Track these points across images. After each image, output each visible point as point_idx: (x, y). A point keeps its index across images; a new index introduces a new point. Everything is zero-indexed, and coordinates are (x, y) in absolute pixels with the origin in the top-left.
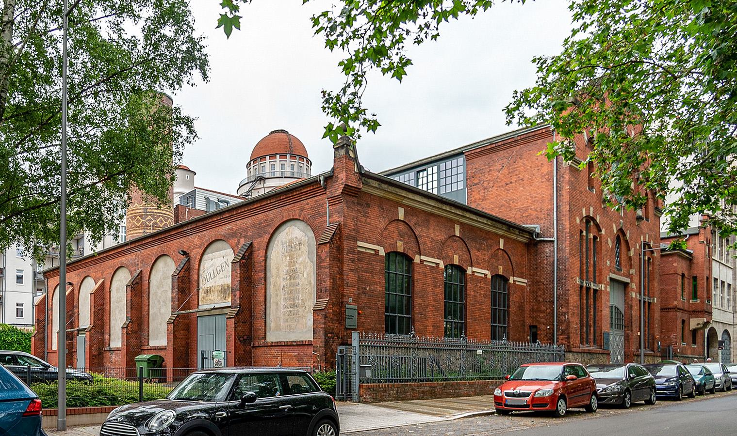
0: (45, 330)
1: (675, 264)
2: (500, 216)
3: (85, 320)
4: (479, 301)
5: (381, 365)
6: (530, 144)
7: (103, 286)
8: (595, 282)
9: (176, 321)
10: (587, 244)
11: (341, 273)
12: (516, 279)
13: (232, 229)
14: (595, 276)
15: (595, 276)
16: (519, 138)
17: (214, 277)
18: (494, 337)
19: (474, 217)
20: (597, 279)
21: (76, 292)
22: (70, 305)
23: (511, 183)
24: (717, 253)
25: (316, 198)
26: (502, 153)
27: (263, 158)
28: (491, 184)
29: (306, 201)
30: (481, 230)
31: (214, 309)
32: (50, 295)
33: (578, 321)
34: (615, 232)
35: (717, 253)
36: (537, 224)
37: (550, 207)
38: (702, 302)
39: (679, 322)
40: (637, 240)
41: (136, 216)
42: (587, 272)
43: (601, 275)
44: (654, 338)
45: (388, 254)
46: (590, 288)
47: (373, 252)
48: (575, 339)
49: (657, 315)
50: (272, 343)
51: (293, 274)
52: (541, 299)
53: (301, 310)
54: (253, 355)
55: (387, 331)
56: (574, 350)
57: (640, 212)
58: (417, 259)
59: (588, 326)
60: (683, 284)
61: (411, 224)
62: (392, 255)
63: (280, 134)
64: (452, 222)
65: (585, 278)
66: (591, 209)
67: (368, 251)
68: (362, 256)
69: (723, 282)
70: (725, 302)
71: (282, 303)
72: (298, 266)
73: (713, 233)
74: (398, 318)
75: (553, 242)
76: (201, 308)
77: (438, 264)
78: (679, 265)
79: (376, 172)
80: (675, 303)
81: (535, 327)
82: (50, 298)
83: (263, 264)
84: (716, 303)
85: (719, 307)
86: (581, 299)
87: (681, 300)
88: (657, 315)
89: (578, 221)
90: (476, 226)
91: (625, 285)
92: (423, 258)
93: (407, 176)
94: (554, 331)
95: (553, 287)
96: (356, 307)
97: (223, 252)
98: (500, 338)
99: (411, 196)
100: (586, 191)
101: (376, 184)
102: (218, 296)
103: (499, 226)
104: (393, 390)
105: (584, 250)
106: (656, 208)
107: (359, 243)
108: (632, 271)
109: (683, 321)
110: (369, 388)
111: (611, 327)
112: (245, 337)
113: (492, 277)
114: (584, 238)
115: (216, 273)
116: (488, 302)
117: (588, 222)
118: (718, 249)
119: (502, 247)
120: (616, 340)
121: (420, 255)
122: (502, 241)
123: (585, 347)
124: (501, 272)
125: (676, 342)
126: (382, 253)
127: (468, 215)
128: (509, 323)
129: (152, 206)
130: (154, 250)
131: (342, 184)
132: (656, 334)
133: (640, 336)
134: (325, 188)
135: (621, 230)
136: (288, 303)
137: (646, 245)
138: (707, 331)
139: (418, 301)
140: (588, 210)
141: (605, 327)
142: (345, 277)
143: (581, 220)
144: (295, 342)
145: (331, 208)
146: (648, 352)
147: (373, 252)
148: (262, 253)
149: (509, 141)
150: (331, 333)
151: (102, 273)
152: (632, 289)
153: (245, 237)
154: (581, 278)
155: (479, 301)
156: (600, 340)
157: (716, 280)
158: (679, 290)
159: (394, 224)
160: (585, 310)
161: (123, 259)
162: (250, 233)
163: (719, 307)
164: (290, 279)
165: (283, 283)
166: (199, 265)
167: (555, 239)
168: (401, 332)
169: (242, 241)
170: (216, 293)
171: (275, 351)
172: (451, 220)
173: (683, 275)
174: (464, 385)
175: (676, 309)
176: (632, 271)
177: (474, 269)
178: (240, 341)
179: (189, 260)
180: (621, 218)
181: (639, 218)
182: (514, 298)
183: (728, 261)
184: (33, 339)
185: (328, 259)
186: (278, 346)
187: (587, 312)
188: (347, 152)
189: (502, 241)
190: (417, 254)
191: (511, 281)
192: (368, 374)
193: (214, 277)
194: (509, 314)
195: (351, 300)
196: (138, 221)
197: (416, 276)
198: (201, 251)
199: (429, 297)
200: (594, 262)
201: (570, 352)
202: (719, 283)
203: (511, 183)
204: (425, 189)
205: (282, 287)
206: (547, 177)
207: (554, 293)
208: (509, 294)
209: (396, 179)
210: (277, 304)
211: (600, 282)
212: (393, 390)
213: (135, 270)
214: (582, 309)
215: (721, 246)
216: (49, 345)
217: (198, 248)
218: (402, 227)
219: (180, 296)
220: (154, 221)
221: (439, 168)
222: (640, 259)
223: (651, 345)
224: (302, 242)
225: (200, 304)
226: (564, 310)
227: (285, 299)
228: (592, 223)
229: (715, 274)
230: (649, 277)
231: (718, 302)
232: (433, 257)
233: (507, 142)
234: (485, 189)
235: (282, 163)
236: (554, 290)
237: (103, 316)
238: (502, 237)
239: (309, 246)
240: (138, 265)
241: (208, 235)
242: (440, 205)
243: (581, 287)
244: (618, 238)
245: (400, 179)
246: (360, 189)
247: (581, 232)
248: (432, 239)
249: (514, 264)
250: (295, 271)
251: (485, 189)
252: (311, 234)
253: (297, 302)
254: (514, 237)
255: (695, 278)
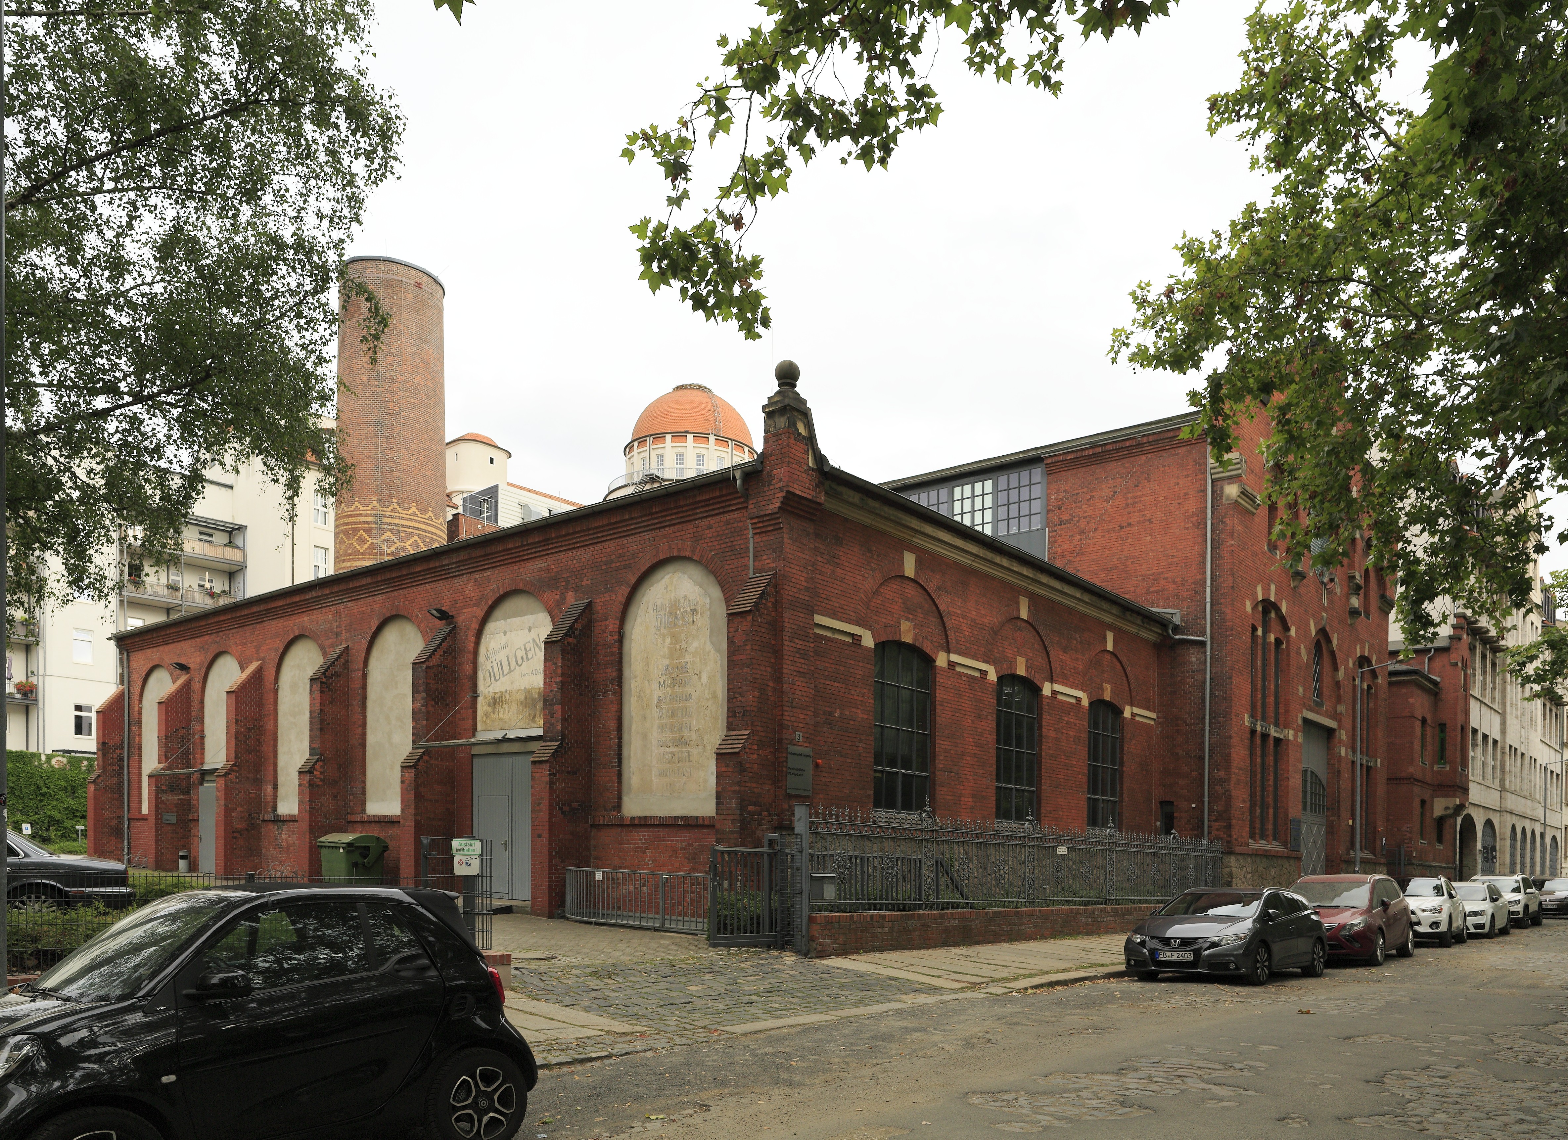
0: (122, 768)
1: (1411, 700)
2: (1109, 587)
3: (216, 751)
4: (966, 740)
5: (863, 872)
6: (1165, 454)
7: (256, 678)
8: (1277, 725)
9: (421, 764)
10: (1264, 654)
11: (778, 677)
12: (1136, 710)
13: (548, 569)
14: (1277, 714)
15: (1277, 714)
16: (1145, 440)
17: (510, 671)
18: (1094, 820)
19: (1057, 584)
20: (1282, 720)
21: (196, 686)
22: (183, 715)
23: (1130, 525)
24: (1478, 684)
25: (727, 517)
26: (1114, 467)
27: (659, 437)
28: (1093, 525)
29: (705, 522)
30: (1070, 610)
31: (504, 740)
32: (136, 689)
33: (1246, 796)
34: (1314, 633)
35: (1478, 684)
36: (1176, 607)
37: (1199, 577)
38: (1454, 770)
39: (1417, 803)
40: (1347, 649)
41: (356, 531)
42: (1264, 705)
43: (1287, 711)
44: (1375, 831)
45: (881, 646)
46: (1268, 735)
47: (849, 640)
48: (1240, 830)
49: (1381, 789)
50: (633, 818)
51: (677, 676)
52: (1181, 752)
53: (695, 752)
54: (593, 843)
55: (877, 804)
56: (1238, 849)
57: (1355, 602)
58: (941, 660)
59: (1264, 806)
60: (1423, 736)
61: (931, 588)
62: (888, 648)
63: (695, 393)
64: (1012, 592)
65: (1259, 715)
66: (1273, 587)
67: (837, 636)
68: (824, 646)
69: (1485, 737)
70: (1489, 770)
71: (655, 736)
72: (688, 658)
73: (1472, 649)
74: (903, 779)
75: (1203, 644)
76: (481, 736)
77: (984, 673)
78: (1419, 703)
79: (875, 482)
80: (1411, 769)
81: (1171, 803)
82: (136, 697)
83: (615, 650)
84: (1475, 773)
85: (1478, 778)
86: (1252, 754)
87: (1421, 764)
88: (1381, 789)
89: (1249, 608)
90: (1052, 596)
91: (1330, 732)
92: (954, 658)
93: (933, 494)
94: (1203, 812)
95: (1203, 730)
96: (808, 751)
97: (529, 619)
98: (1104, 825)
99: (929, 529)
100: (1264, 553)
101: (855, 497)
102: (519, 713)
103: (1105, 605)
104: (882, 927)
105: (1259, 663)
106: (1383, 597)
107: (819, 619)
108: (1341, 708)
109: (1423, 802)
110: (829, 922)
111: (1305, 809)
112: (575, 805)
113: (1091, 704)
114: (1260, 641)
115: (513, 664)
116: (1083, 752)
117: (1265, 612)
118: (1479, 677)
119: (1110, 647)
120: (1312, 833)
121: (948, 651)
122: (1110, 637)
123: (1262, 845)
124: (1107, 697)
125: (1411, 839)
126: (868, 641)
127: (1044, 579)
128: (1121, 795)
129: (394, 510)
130: (377, 604)
131: (781, 489)
132: (1379, 823)
133: (1353, 828)
134: (746, 495)
135: (1323, 632)
136: (668, 735)
137: (1364, 661)
138: (1459, 820)
139: (942, 744)
140: (1266, 589)
141: (1294, 810)
142: (786, 687)
143: (1254, 608)
144: (682, 818)
145: (758, 538)
146: (1368, 855)
147: (849, 640)
148: (612, 625)
149: (1128, 444)
150: (755, 804)
151: (258, 649)
152: (1340, 741)
153: (576, 589)
154: (1252, 716)
155: (1064, 752)
156: (1286, 832)
157: (1475, 731)
158: (1417, 746)
159: (894, 585)
160: (1259, 776)
161: (305, 620)
162: (586, 582)
163: (1478, 778)
164: (673, 685)
165: (657, 693)
166: (477, 643)
167: (1207, 638)
168: (907, 806)
169: (570, 597)
170: (514, 707)
171: (639, 837)
172: (1011, 587)
173: (1424, 721)
174: (1030, 914)
175: (1412, 780)
176: (1341, 708)
177: (1057, 687)
178: (563, 813)
179: (453, 631)
180: (1324, 609)
181: (1354, 613)
182: (1132, 748)
183: (1493, 699)
184: (92, 788)
185: (748, 647)
186: (646, 826)
187: (1263, 779)
188: (792, 424)
189: (1110, 637)
190: (943, 649)
191: (1127, 714)
192: (830, 892)
193: (510, 671)
194: (1121, 778)
195: (799, 736)
196: (362, 541)
197: (940, 695)
198: (480, 613)
199: (966, 740)
200: (1277, 686)
201: (1231, 853)
202: (1480, 737)
203: (1130, 525)
204: (967, 522)
205: (655, 700)
206: (1194, 519)
207: (1203, 743)
208: (1122, 739)
209: (914, 498)
210: (645, 736)
211: (1287, 726)
212: (882, 927)
213: (332, 646)
214: (1253, 774)
215: (1484, 673)
216: (134, 804)
217: (474, 605)
218: (911, 591)
219: (431, 709)
220: (398, 544)
221: (995, 486)
222: (1354, 686)
223: (1370, 843)
224: (699, 607)
225: (479, 727)
226: (1222, 774)
227: (662, 727)
228: (1273, 615)
229: (1474, 723)
230: (1369, 718)
231: (1478, 771)
232: (975, 657)
233: (1123, 445)
234: (1082, 532)
235: (698, 451)
236: (1203, 736)
237: (259, 742)
238: (1112, 628)
239: (712, 616)
240: (339, 634)
241: (496, 579)
242: (989, 555)
243: (1253, 732)
244: (1318, 645)
245: (921, 499)
246: (820, 504)
247: (1254, 629)
248: (973, 620)
249: (1132, 681)
250: (682, 668)
251: (1082, 532)
252: (716, 593)
253: (686, 734)
254: (1133, 629)
255: (1442, 727)
